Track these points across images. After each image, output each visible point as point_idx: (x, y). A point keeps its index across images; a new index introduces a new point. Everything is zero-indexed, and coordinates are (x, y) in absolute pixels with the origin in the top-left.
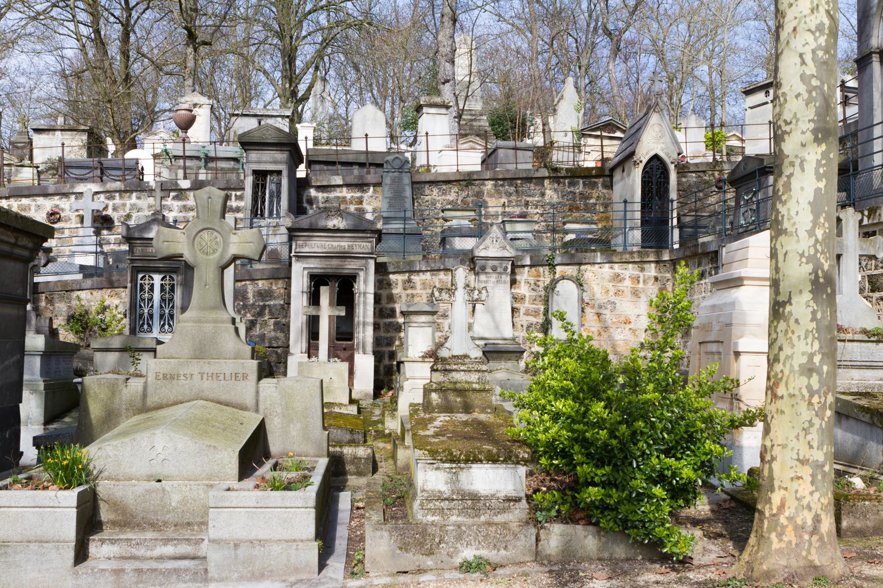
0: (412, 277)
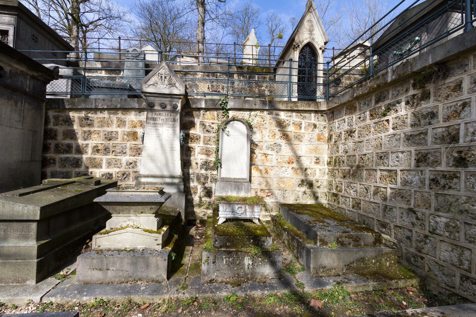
0: (89, 115)
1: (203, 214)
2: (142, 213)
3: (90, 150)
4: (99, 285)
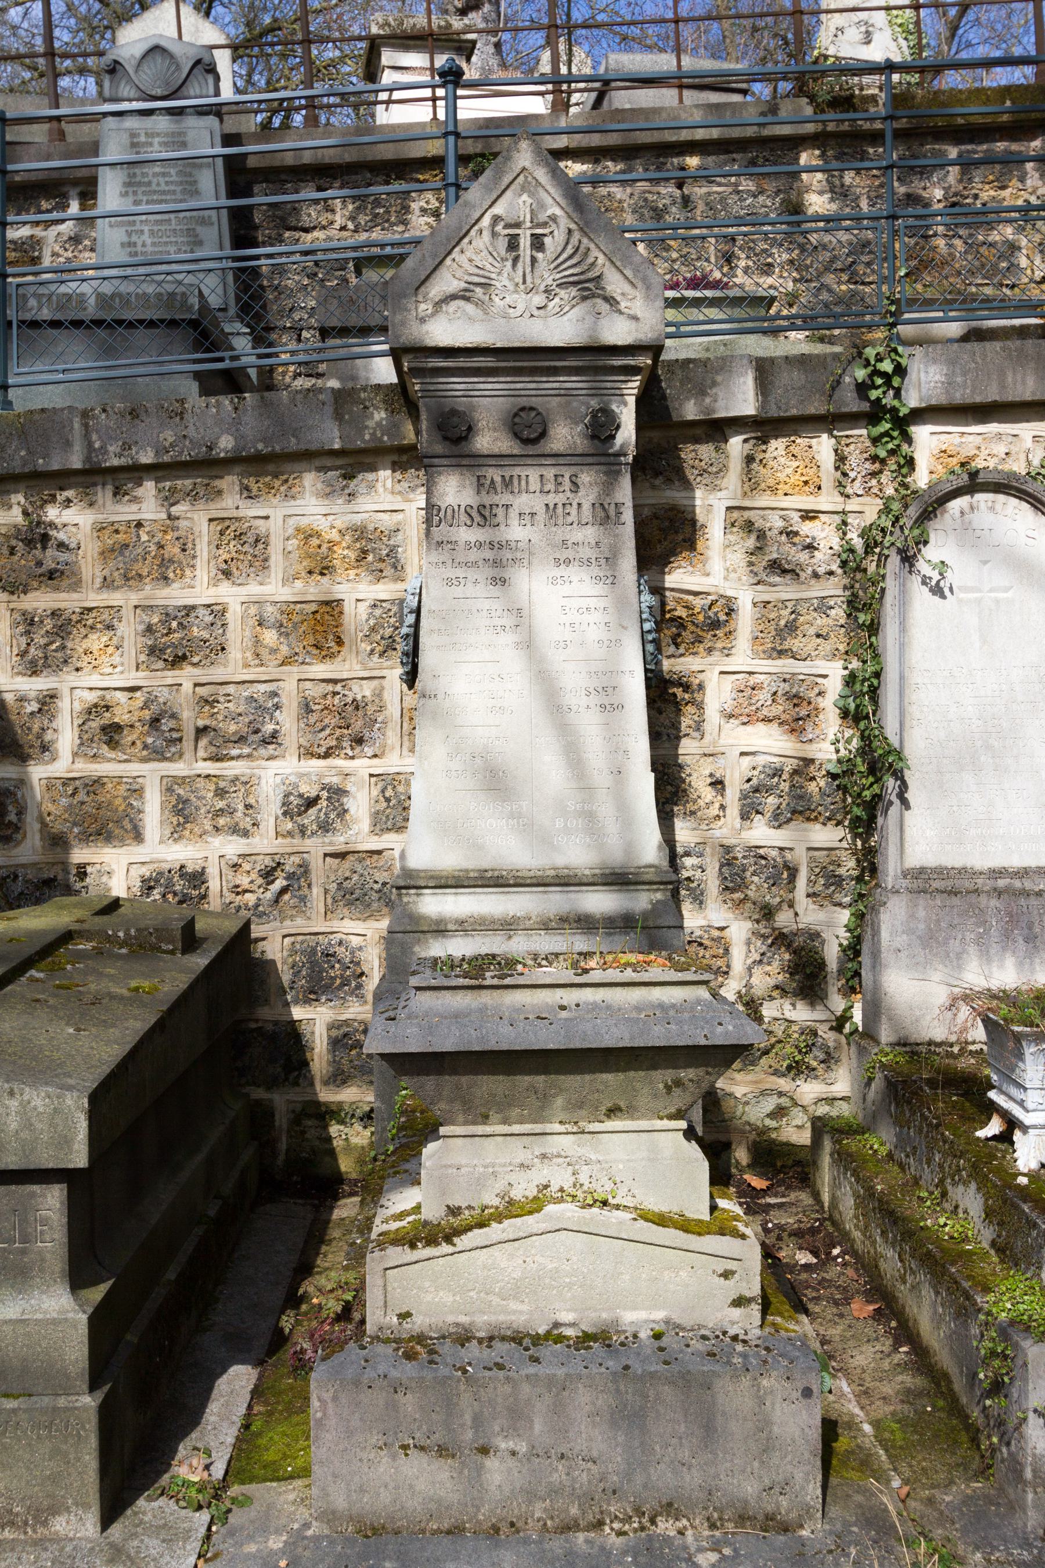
0: (52, 513)
1: (770, 1104)
2: (613, 1112)
3: (65, 736)
4: (446, 1540)
